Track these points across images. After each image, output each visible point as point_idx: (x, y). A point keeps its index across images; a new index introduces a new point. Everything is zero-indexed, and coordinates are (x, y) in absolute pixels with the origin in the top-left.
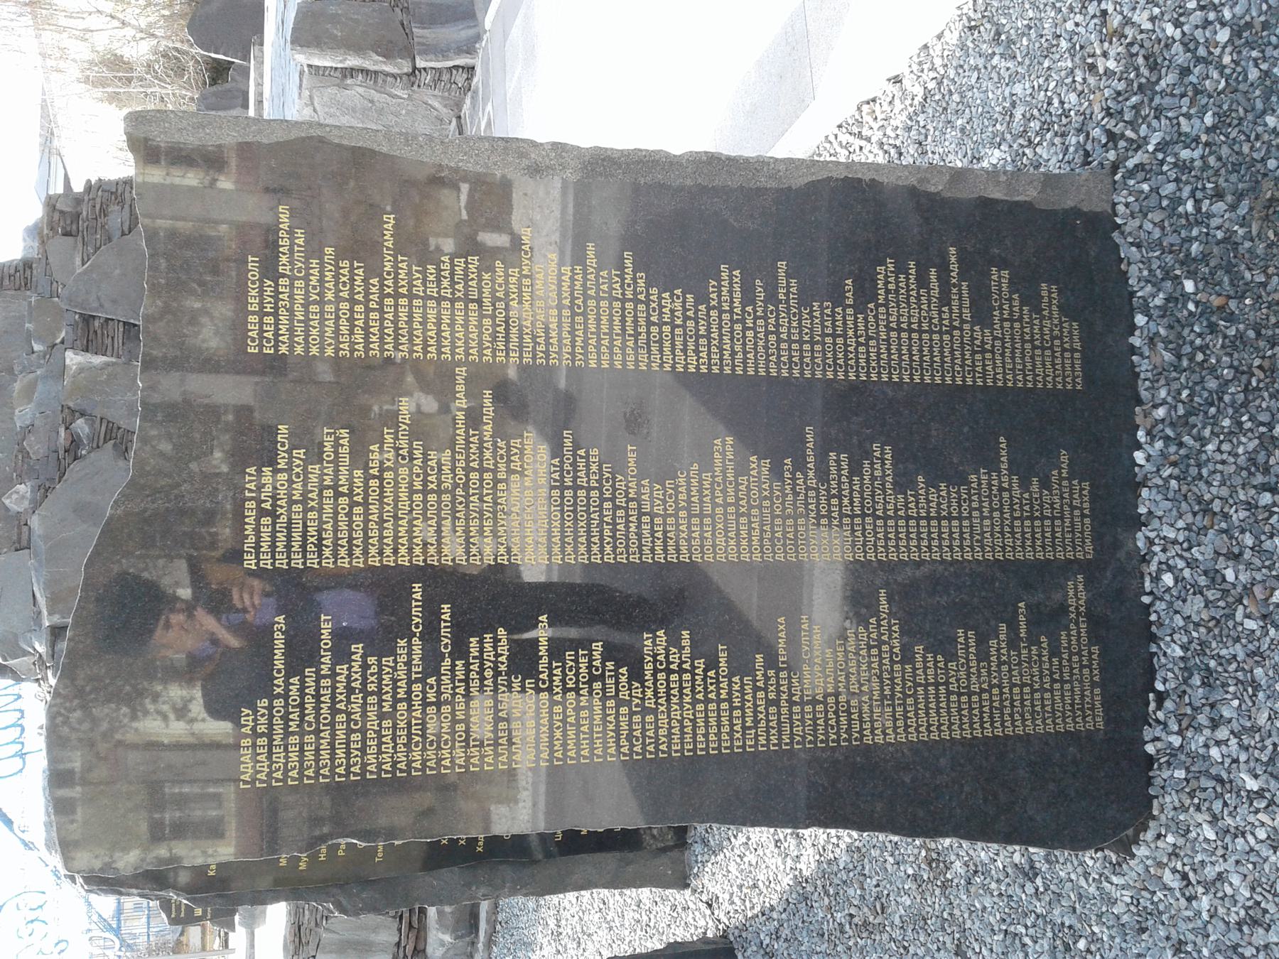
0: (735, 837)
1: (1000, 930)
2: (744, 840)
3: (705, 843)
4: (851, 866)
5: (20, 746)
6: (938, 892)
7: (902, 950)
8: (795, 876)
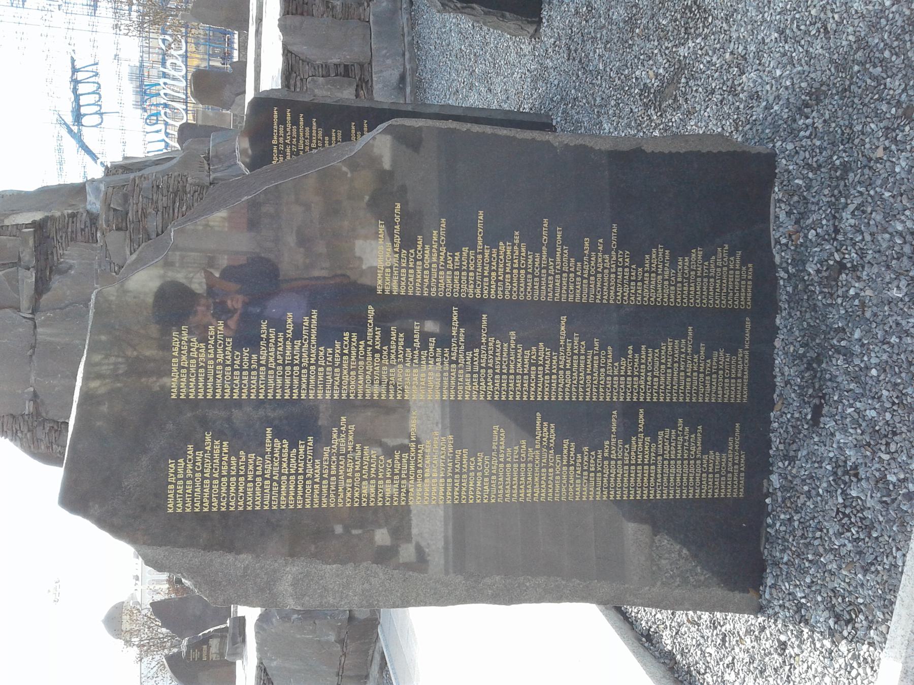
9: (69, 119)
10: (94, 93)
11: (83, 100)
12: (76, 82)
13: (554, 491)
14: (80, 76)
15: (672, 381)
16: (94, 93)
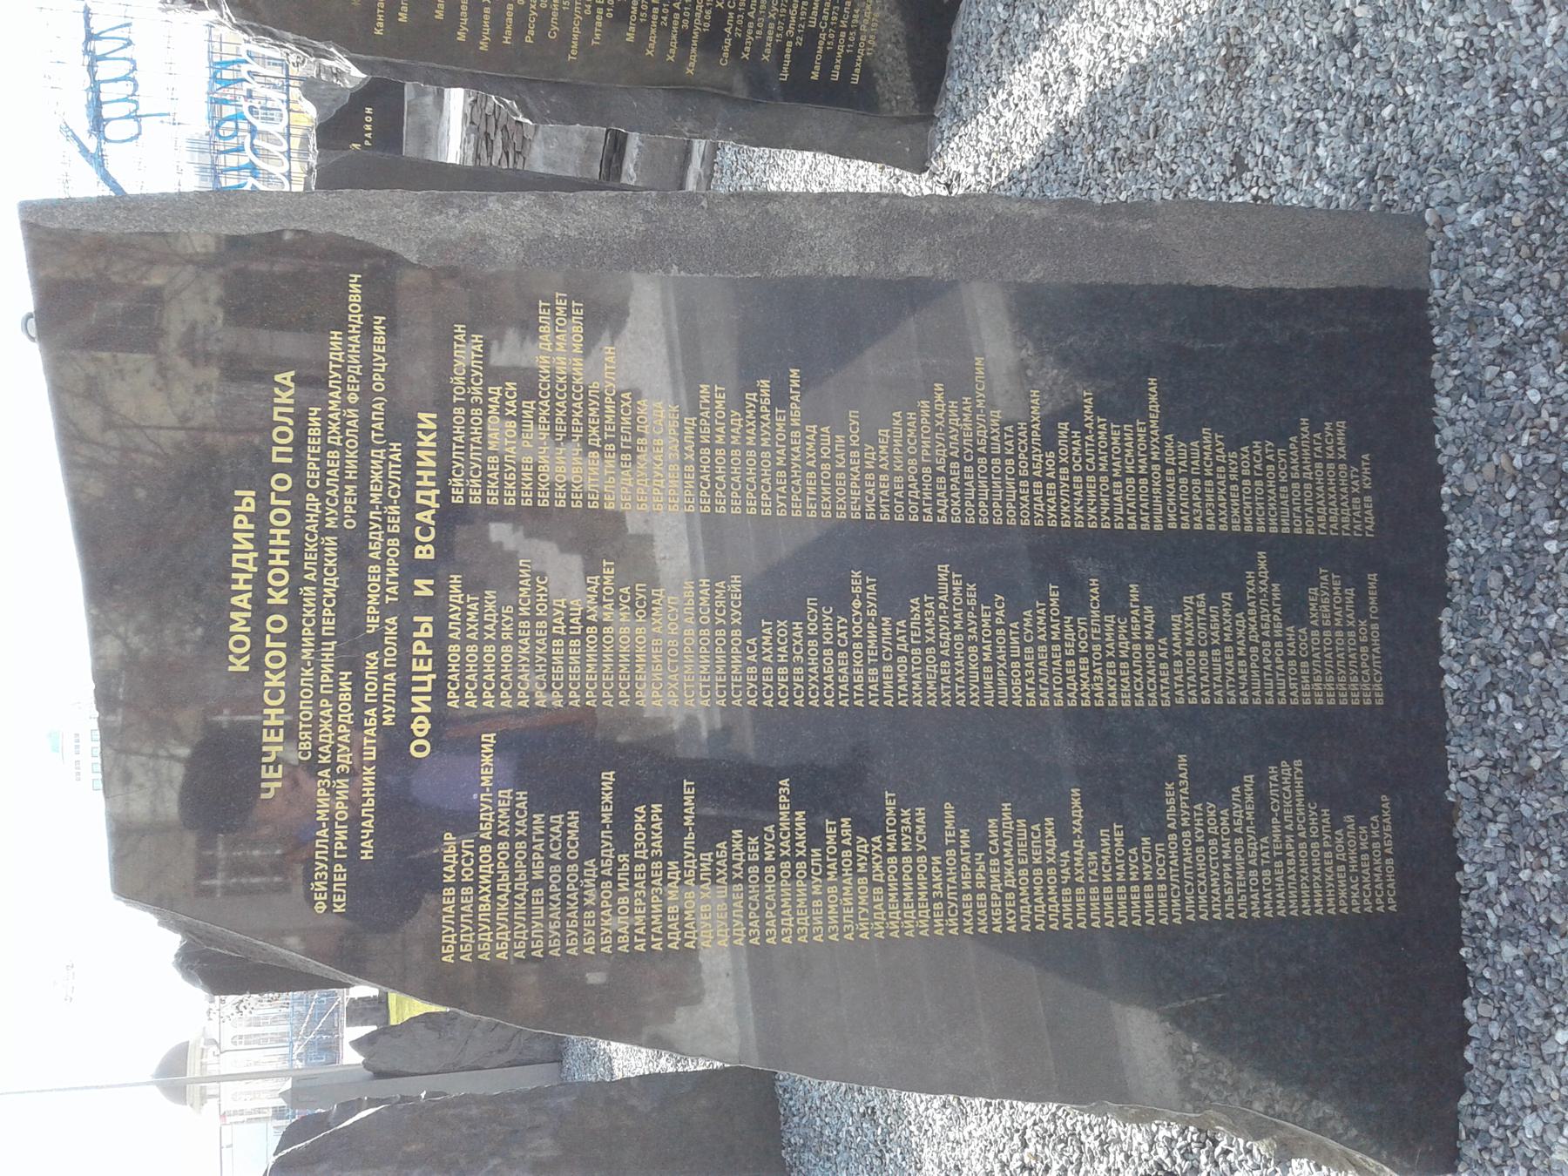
0: (994, 96)
1: (1292, 120)
2: (1005, 96)
3: (956, 112)
4: (1130, 90)
5: (133, 107)
6: (1229, 94)
7: (1168, 175)
8: (1059, 122)
9: (82, 125)
10: (125, 78)
11: (107, 92)
12: (94, 60)
13: (1301, 460)
14: (100, 47)
15: (1074, 912)
16: (125, 78)
